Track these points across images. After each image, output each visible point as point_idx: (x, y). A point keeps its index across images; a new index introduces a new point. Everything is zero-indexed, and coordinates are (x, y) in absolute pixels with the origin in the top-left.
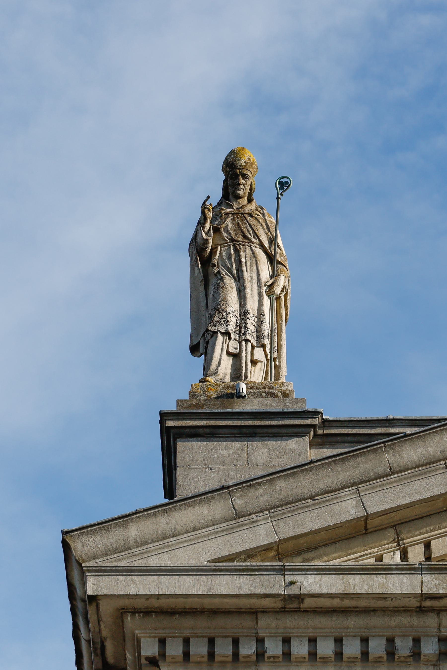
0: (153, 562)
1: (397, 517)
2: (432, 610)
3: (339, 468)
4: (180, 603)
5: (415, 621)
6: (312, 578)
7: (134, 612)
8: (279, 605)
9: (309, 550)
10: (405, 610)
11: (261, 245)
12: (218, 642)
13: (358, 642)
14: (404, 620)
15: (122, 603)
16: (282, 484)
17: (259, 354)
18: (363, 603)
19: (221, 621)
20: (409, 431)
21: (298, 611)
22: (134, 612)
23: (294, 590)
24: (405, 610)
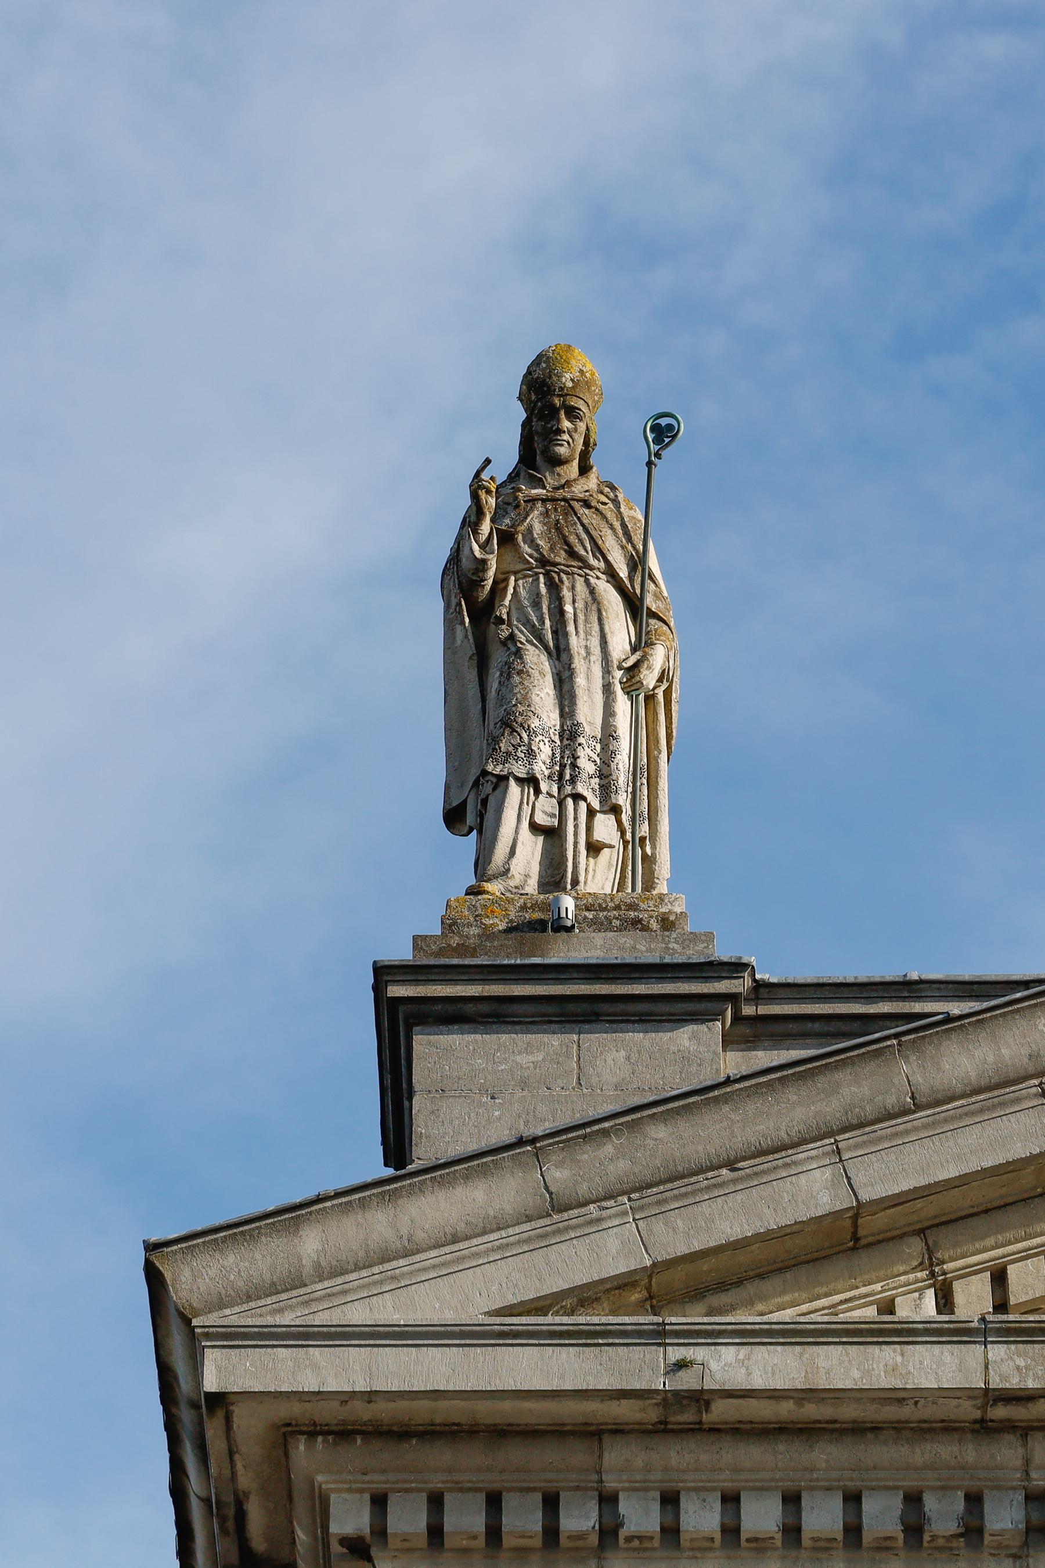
0: (357, 1314)
1: (927, 1209)
2: (1009, 1427)
3: (792, 1094)
4: (422, 1412)
5: (970, 1453)
6: (729, 1354)
7: (314, 1431)
8: (652, 1415)
9: (722, 1286)
10: (948, 1428)
11: (611, 574)
12: (510, 1502)
13: (836, 1503)
14: (945, 1450)
15: (285, 1411)
16: (659, 1132)
17: (605, 828)
18: (848, 1412)
19: (516, 1454)
20: (956, 1008)
21: (697, 1429)
22: (314, 1431)
23: (686, 1381)
24: (948, 1428)
